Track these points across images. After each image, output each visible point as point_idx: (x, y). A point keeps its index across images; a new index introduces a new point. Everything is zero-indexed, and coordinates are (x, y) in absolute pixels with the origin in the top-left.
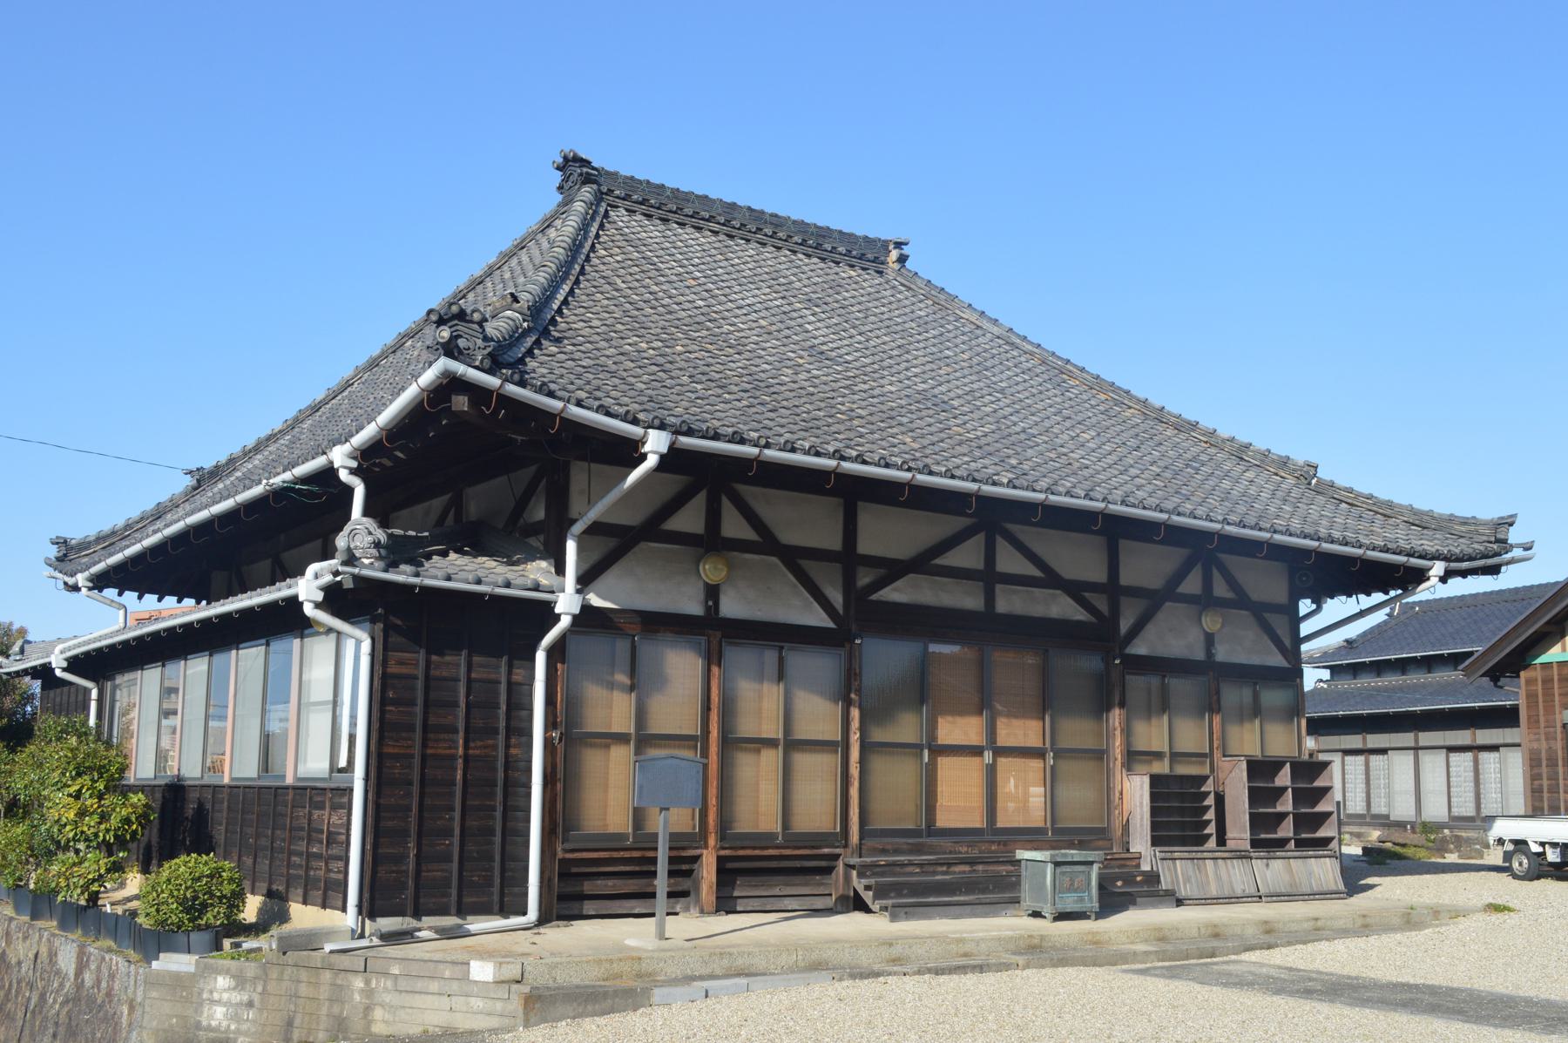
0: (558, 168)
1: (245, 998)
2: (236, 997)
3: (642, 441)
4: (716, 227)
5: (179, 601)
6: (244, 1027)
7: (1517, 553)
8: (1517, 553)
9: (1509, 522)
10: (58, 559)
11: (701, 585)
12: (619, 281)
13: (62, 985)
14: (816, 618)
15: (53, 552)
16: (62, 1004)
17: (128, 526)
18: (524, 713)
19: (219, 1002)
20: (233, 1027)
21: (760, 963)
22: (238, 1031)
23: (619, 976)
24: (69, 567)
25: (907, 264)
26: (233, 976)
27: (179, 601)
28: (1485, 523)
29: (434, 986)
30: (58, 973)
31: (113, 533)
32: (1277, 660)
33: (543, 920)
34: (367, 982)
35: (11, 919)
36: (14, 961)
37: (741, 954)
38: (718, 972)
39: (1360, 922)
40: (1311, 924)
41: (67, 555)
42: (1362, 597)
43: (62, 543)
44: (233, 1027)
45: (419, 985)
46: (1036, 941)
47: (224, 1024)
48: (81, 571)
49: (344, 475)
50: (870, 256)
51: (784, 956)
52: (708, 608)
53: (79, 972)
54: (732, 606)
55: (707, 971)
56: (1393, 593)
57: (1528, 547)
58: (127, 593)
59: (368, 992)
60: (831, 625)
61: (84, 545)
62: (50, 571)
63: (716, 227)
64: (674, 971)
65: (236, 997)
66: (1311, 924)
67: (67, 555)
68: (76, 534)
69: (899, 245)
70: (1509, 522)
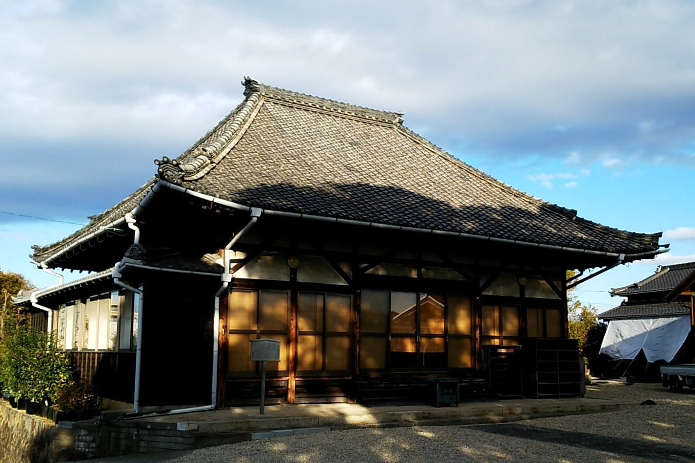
0: (243, 84)
1: (92, 438)
2: (88, 438)
3: (250, 212)
4: (315, 110)
5: (89, 273)
6: (91, 450)
7: (661, 249)
8: (661, 249)
9: (660, 235)
10: (35, 255)
11: (289, 268)
12: (262, 138)
13: (26, 436)
14: (342, 283)
15: (33, 252)
16: (26, 444)
17: (64, 241)
18: (210, 322)
19: (82, 441)
20: (87, 450)
21: (302, 423)
22: (88, 452)
23: (240, 429)
24: (39, 259)
25: (403, 124)
26: (87, 430)
27: (89, 273)
28: (648, 236)
29: (163, 433)
30: (25, 430)
31: (58, 244)
32: (556, 297)
33: (216, 408)
34: (138, 432)
35: (10, 409)
36: (10, 427)
37: (294, 420)
38: (283, 427)
39: (580, 408)
40: (556, 409)
41: (38, 253)
42: (591, 269)
43: (36, 248)
44: (87, 450)
45: (158, 432)
46: (426, 415)
47: (84, 449)
48: (43, 261)
49: (131, 226)
50: (387, 121)
51: (313, 420)
52: (291, 278)
53: (32, 430)
54: (301, 278)
55: (279, 427)
56: (604, 268)
57: (667, 246)
58: (65, 270)
59: (138, 436)
60: (347, 284)
61: (45, 249)
62: (32, 260)
63: (315, 110)
64: (264, 426)
65: (88, 438)
66: (556, 409)
67: (38, 253)
68: (42, 245)
69: (400, 115)
70: (660, 235)
